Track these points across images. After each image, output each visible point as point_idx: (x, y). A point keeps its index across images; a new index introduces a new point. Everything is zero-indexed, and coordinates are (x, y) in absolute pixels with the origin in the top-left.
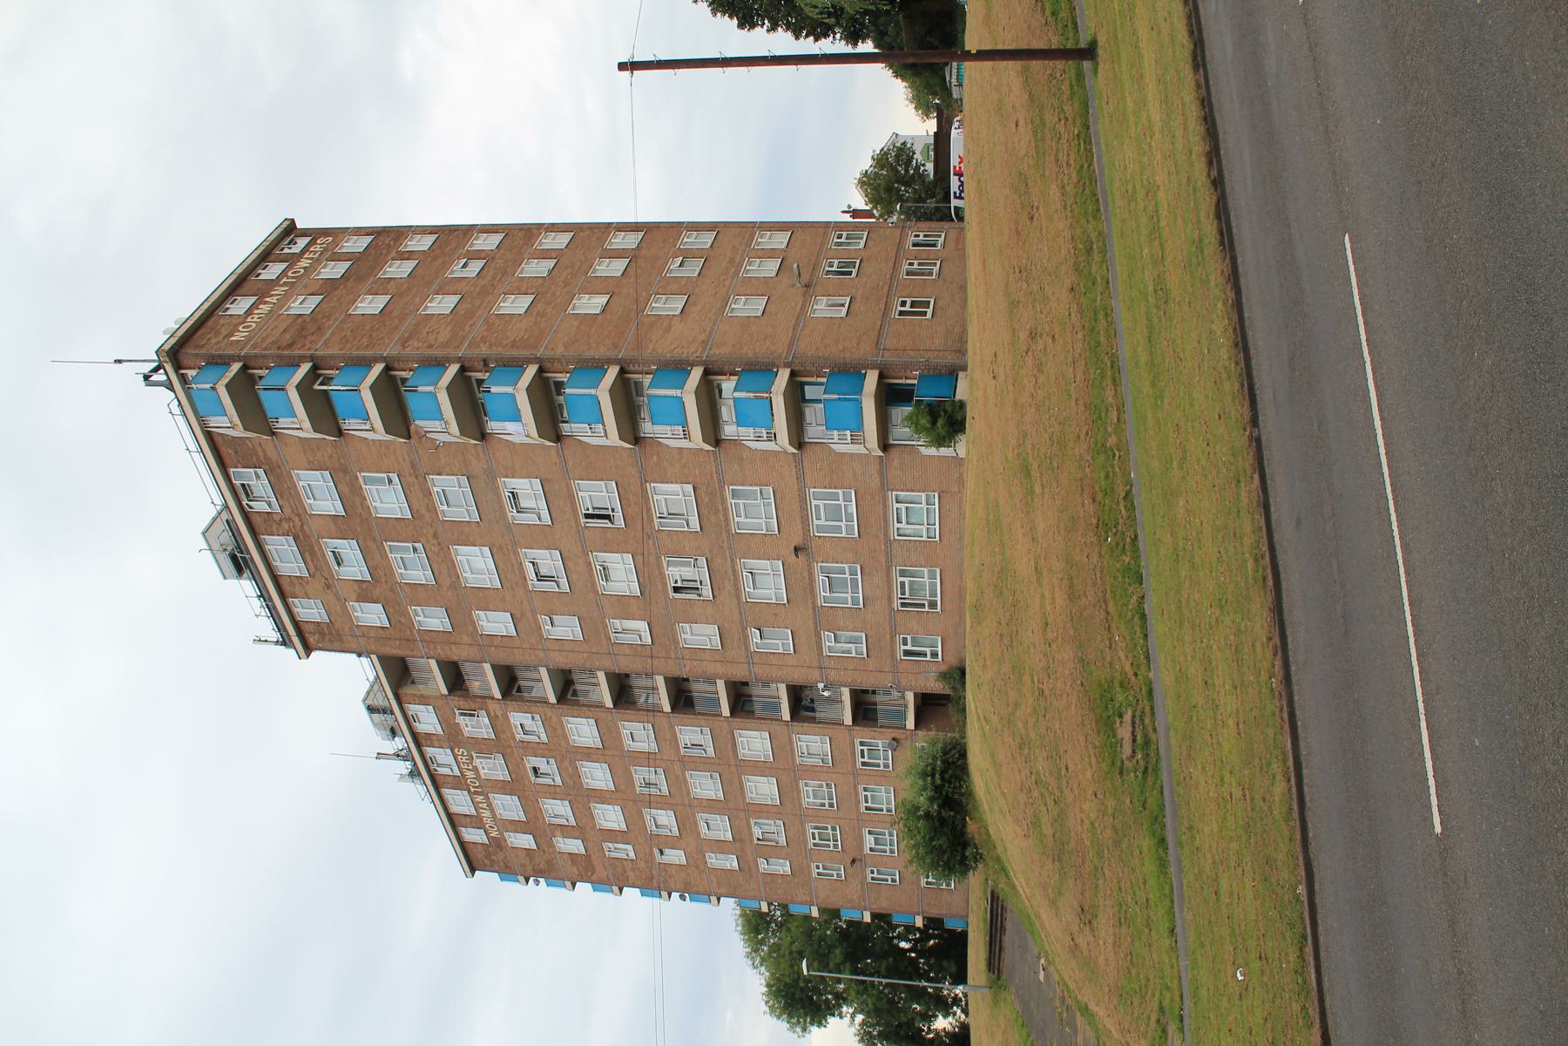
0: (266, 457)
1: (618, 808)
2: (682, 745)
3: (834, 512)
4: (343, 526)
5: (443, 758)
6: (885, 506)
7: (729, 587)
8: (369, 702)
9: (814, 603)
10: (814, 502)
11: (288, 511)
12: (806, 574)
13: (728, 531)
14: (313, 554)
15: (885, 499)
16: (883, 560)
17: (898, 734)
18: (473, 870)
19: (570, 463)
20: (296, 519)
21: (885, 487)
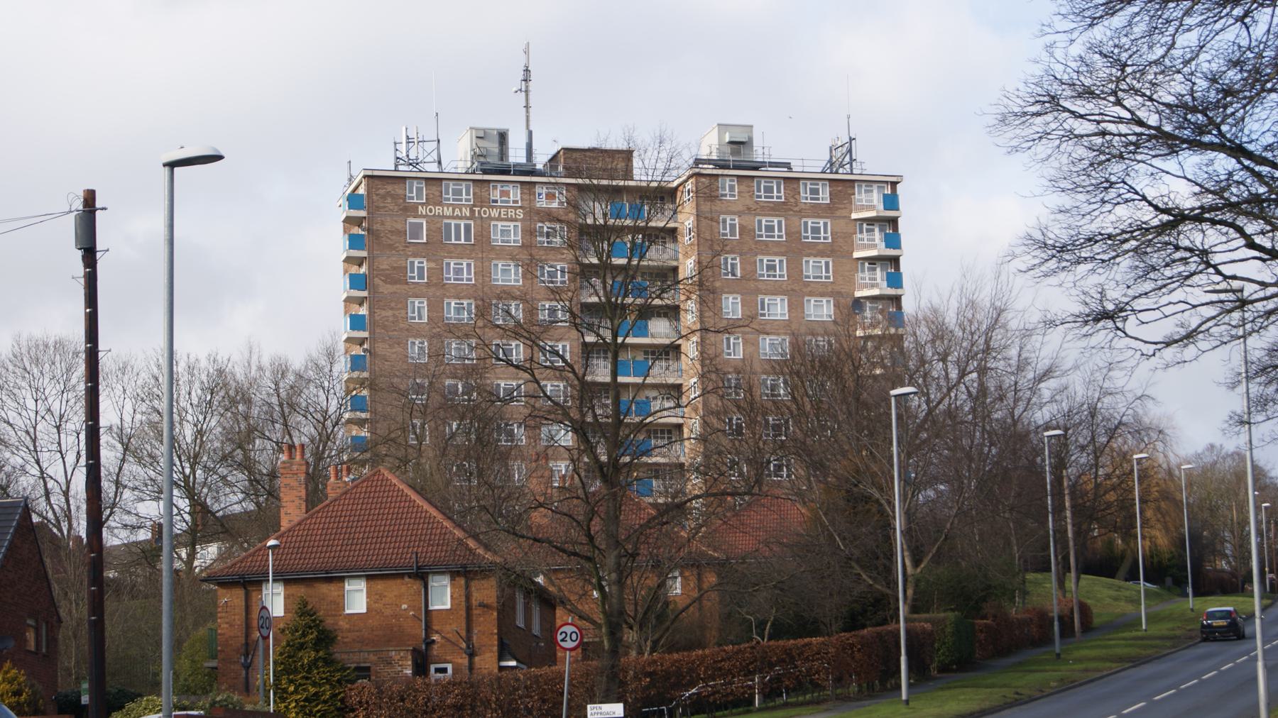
0: (838, 209)
14: (772, 209)
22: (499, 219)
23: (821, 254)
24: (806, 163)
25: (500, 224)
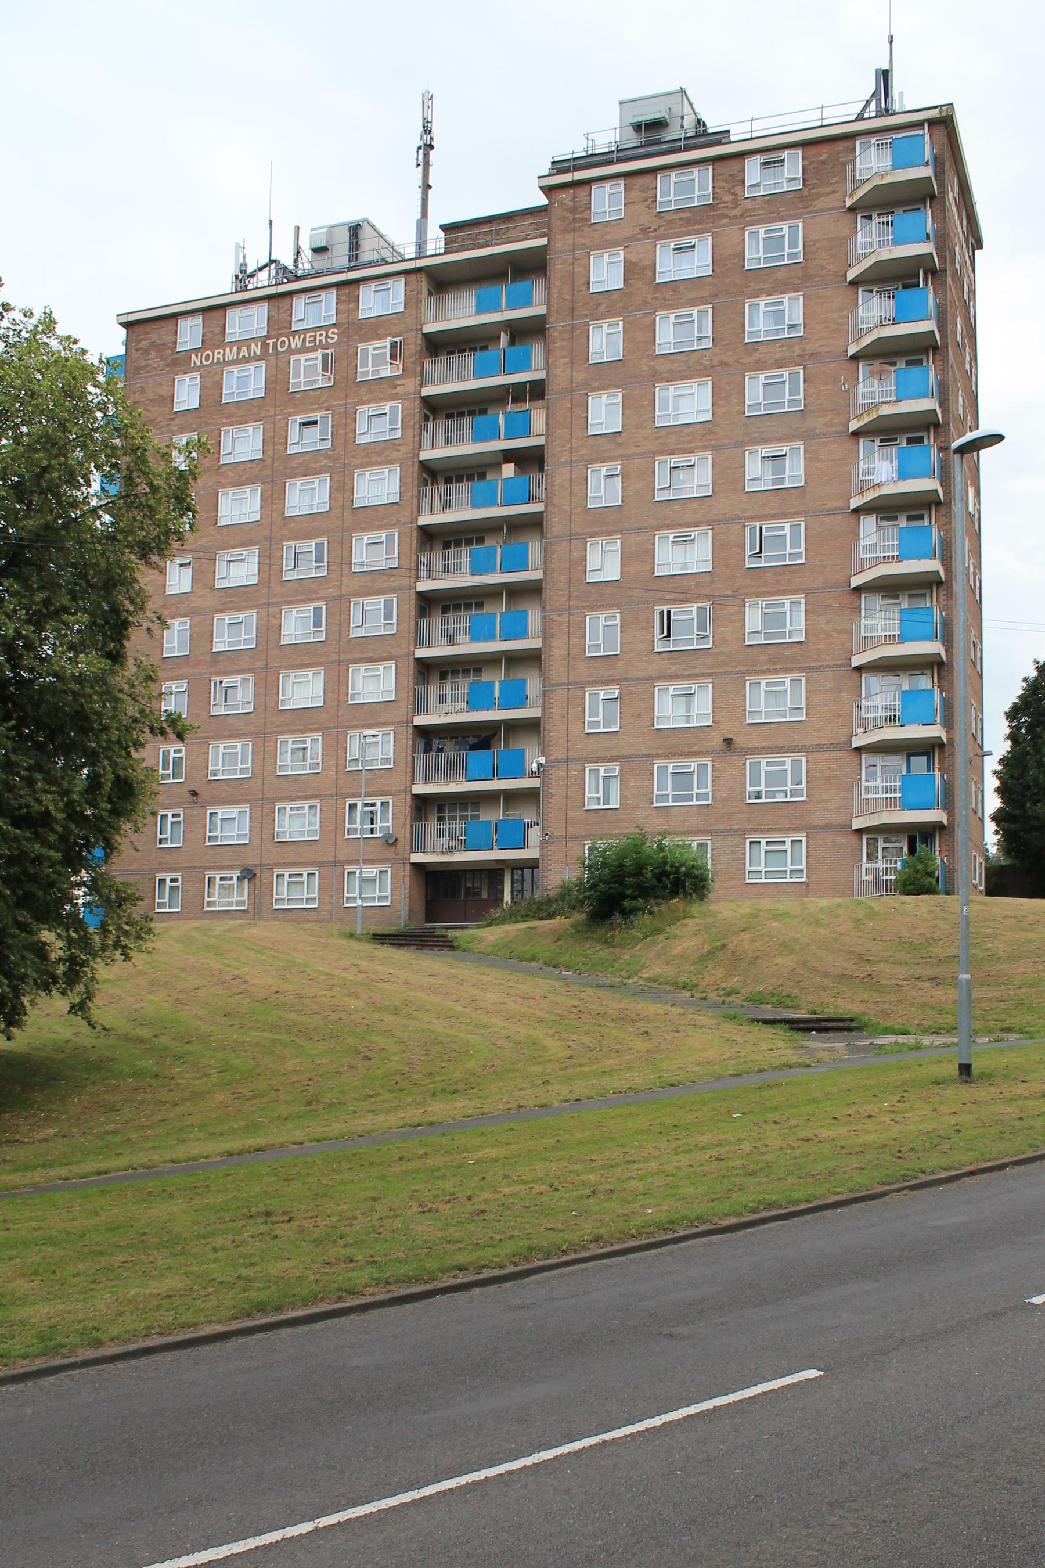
0: (818, 196)
1: (257, 517)
2: (367, 600)
3: (778, 778)
4: (729, 261)
5: (315, 313)
6: (788, 830)
7: (674, 669)
8: (365, 225)
9: (658, 756)
10: (788, 761)
11: (748, 204)
12: (695, 748)
13: (749, 673)
14: (688, 222)
15: (795, 830)
16: (721, 827)
17: (404, 843)
18: (128, 325)
19: (826, 519)
20: (736, 212)
21: (811, 830)
22: (304, 350)
23: (782, 287)
24: (827, 113)
25: (302, 357)
